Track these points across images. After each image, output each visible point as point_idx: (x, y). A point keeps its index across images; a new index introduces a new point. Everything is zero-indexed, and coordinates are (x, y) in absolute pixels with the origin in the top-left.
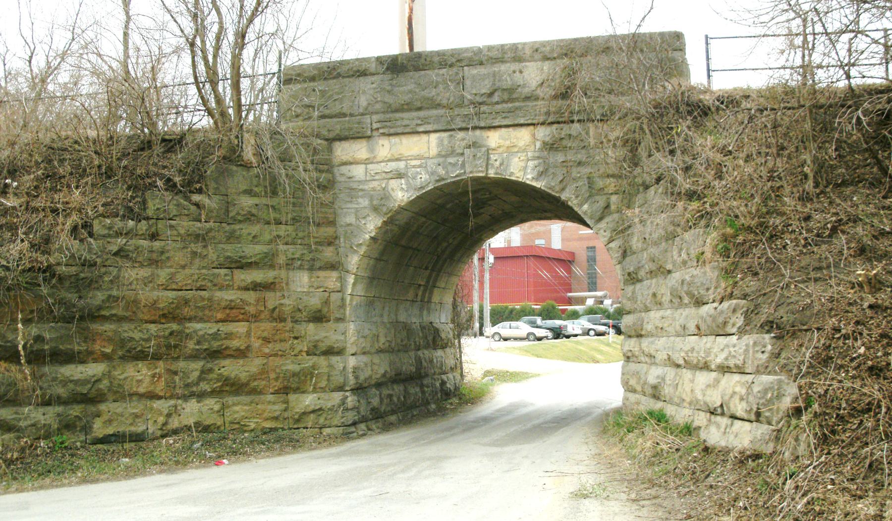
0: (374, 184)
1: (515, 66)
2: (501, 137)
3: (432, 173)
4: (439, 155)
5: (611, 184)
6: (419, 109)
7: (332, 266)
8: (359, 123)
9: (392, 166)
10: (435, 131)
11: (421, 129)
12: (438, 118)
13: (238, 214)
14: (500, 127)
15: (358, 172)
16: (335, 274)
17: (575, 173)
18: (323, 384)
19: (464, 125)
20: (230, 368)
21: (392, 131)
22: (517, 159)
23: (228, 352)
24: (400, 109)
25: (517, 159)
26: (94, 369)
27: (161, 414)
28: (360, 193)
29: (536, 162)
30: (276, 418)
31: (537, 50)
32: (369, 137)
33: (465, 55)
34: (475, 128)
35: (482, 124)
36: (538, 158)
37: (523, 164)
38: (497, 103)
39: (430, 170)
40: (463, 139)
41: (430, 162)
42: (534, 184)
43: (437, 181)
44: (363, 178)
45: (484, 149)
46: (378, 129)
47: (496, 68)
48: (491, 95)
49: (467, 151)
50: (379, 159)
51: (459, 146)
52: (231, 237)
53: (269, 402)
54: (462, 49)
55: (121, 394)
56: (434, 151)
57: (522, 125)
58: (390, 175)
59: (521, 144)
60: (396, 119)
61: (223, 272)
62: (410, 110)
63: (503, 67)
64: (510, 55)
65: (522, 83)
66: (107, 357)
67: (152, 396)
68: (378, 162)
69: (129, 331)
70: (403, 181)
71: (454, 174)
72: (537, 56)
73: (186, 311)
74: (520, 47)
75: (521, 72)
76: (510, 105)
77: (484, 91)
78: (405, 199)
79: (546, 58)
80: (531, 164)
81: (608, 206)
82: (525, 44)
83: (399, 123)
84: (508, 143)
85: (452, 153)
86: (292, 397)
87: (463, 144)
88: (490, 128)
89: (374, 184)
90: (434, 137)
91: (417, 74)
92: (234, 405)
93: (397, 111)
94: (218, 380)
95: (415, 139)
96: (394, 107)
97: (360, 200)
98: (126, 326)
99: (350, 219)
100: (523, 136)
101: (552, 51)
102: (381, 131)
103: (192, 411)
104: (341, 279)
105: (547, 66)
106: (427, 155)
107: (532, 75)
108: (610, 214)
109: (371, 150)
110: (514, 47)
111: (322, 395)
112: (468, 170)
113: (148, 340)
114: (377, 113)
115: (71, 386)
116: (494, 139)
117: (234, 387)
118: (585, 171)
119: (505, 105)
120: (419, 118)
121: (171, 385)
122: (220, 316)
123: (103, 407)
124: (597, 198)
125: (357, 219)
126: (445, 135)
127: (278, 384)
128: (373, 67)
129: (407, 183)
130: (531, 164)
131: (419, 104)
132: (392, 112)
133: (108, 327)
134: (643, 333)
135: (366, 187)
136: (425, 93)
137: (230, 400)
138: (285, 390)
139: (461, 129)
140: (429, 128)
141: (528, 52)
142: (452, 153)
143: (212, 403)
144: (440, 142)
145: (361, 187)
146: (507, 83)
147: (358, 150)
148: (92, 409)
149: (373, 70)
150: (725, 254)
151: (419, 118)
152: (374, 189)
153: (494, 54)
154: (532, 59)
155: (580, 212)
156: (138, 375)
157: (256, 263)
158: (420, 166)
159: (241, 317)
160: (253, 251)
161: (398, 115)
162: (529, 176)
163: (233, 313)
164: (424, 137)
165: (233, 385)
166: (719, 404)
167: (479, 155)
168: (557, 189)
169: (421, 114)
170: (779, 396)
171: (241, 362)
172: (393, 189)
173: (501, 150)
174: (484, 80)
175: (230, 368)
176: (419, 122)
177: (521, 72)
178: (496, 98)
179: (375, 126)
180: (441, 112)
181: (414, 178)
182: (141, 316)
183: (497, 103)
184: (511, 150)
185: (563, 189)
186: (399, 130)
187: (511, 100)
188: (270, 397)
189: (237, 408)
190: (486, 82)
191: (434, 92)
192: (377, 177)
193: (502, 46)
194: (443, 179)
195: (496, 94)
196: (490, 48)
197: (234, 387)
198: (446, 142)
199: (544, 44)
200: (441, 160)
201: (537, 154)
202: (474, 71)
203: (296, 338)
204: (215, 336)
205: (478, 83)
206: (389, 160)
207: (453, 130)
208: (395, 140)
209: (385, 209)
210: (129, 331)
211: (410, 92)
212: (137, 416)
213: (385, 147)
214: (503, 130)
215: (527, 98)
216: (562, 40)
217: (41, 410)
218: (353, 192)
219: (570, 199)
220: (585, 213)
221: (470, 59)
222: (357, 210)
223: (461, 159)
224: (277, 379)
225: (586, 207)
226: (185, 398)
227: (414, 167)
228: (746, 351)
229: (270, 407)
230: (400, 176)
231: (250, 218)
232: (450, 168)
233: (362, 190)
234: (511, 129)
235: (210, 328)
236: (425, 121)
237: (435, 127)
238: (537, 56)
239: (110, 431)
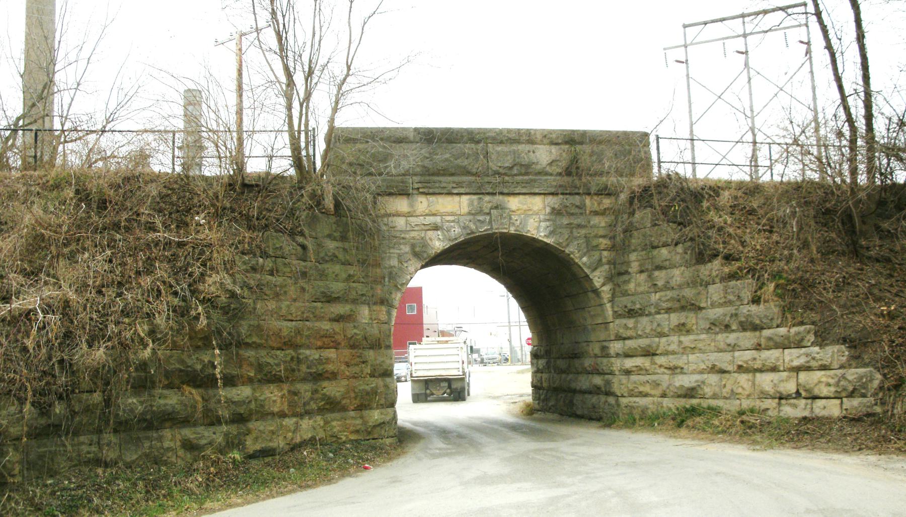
0: (413, 234)
1: (528, 147)
2: (520, 202)
3: (464, 228)
4: (469, 213)
5: (604, 242)
6: (452, 175)
7: (383, 302)
8: (402, 182)
9: (430, 220)
10: (466, 194)
11: (455, 191)
12: (470, 184)
13: (326, 255)
14: (519, 194)
15: (400, 222)
16: (384, 308)
17: (575, 234)
18: (382, 401)
19: (491, 191)
20: (332, 389)
21: (431, 191)
22: (532, 220)
23: (326, 375)
24: (437, 173)
25: (532, 220)
26: (245, 391)
27: (290, 431)
28: (402, 241)
29: (548, 223)
30: (357, 432)
31: (545, 136)
32: (409, 195)
33: (490, 134)
34: (502, 193)
35: (506, 191)
36: (548, 220)
37: (536, 224)
38: (516, 175)
39: (462, 224)
40: (490, 202)
41: (462, 219)
42: (545, 240)
43: (469, 234)
44: (404, 228)
45: (507, 211)
46: (418, 189)
47: (515, 147)
48: (511, 168)
49: (494, 212)
50: (418, 213)
51: (486, 207)
52: (323, 275)
53: (353, 418)
54: (486, 129)
55: (263, 414)
56: (465, 209)
57: (535, 194)
58: (428, 227)
59: (536, 208)
60: (432, 180)
61: (319, 305)
62: (444, 175)
63: (521, 147)
64: (525, 138)
65: (535, 161)
66: (250, 381)
67: (283, 415)
68: (417, 216)
69: (264, 356)
70: (439, 233)
71: (483, 229)
72: (546, 141)
73: (298, 340)
74: (533, 132)
75: (534, 152)
76: (526, 178)
77: (507, 165)
78: (441, 248)
79: (552, 143)
80: (543, 224)
81: (600, 260)
82: (536, 130)
83: (437, 185)
84: (525, 207)
85: (480, 212)
86: (366, 413)
87: (489, 205)
88: (509, 194)
89: (413, 234)
90: (465, 199)
91: (450, 146)
92: (332, 420)
93: (433, 174)
94: (323, 400)
95: (449, 199)
96: (431, 171)
97: (402, 246)
98: (263, 353)
99: (394, 262)
100: (537, 203)
101: (558, 138)
102: (421, 190)
103: (307, 427)
104: (389, 313)
105: (554, 149)
106: (459, 213)
107: (543, 156)
108: (602, 265)
109: (411, 206)
110: (528, 132)
111: (383, 411)
112: (495, 226)
113: (278, 365)
114: (416, 175)
115: (233, 407)
116: (514, 203)
117: (332, 406)
118: (583, 232)
119: (521, 177)
120: (454, 182)
121: (292, 404)
122: (319, 343)
123: (251, 425)
124: (593, 253)
125: (400, 262)
126: (475, 197)
127: (357, 402)
128: (411, 136)
129: (444, 235)
130: (543, 224)
131: (453, 171)
132: (429, 175)
133: (250, 354)
134: (658, 352)
135: (407, 236)
136: (459, 162)
137: (329, 416)
138: (361, 408)
139: (488, 194)
140: (462, 191)
141: (539, 137)
142: (480, 212)
143: (319, 420)
144: (471, 203)
145: (403, 236)
146: (525, 160)
147: (401, 204)
148: (243, 429)
149: (412, 138)
150: (781, 297)
151: (454, 182)
152: (413, 238)
153: (512, 136)
154: (542, 143)
155: (580, 263)
156: (273, 396)
157: (338, 298)
158: (453, 221)
159: (332, 344)
160: (337, 287)
161: (436, 178)
162: (542, 234)
163: (330, 341)
164: (457, 198)
165: (331, 403)
166: (794, 391)
167: (504, 215)
168: (564, 244)
169: (456, 179)
170: (871, 380)
171: (334, 383)
172: (431, 239)
173: (519, 212)
174: (507, 156)
175: (332, 389)
176: (454, 185)
177: (534, 152)
178: (515, 171)
179: (416, 186)
180: (472, 178)
181: (448, 231)
182: (271, 343)
183: (516, 175)
184: (528, 213)
185: (568, 245)
186: (437, 191)
187: (527, 174)
188: (352, 413)
189: (334, 423)
190: (509, 158)
191: (466, 163)
192: (416, 228)
193: (519, 130)
194: (473, 233)
195: (515, 168)
196: (509, 131)
197: (332, 406)
198: (476, 203)
199: (551, 132)
200: (471, 217)
201: (547, 217)
202: (499, 148)
203: (363, 362)
204: (320, 361)
205: (500, 157)
206: (427, 215)
207: (483, 194)
208: (432, 198)
209: (425, 255)
210: (264, 356)
211: (446, 160)
212: (273, 432)
213: (422, 203)
214: (521, 197)
215: (539, 173)
216: (563, 131)
217: (212, 429)
218: (395, 238)
219: (572, 253)
220: (584, 264)
221: (494, 139)
222: (399, 256)
223: (488, 218)
224: (355, 398)
225: (585, 259)
226: (301, 416)
227: (448, 221)
228: (832, 356)
229: (354, 422)
230: (436, 228)
231: (334, 259)
232: (478, 224)
233: (403, 238)
234: (527, 197)
235: (314, 354)
236: (459, 185)
237: (468, 191)
238: (546, 141)
239: (258, 447)
